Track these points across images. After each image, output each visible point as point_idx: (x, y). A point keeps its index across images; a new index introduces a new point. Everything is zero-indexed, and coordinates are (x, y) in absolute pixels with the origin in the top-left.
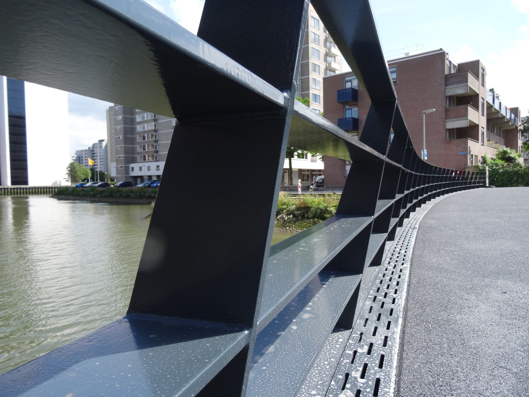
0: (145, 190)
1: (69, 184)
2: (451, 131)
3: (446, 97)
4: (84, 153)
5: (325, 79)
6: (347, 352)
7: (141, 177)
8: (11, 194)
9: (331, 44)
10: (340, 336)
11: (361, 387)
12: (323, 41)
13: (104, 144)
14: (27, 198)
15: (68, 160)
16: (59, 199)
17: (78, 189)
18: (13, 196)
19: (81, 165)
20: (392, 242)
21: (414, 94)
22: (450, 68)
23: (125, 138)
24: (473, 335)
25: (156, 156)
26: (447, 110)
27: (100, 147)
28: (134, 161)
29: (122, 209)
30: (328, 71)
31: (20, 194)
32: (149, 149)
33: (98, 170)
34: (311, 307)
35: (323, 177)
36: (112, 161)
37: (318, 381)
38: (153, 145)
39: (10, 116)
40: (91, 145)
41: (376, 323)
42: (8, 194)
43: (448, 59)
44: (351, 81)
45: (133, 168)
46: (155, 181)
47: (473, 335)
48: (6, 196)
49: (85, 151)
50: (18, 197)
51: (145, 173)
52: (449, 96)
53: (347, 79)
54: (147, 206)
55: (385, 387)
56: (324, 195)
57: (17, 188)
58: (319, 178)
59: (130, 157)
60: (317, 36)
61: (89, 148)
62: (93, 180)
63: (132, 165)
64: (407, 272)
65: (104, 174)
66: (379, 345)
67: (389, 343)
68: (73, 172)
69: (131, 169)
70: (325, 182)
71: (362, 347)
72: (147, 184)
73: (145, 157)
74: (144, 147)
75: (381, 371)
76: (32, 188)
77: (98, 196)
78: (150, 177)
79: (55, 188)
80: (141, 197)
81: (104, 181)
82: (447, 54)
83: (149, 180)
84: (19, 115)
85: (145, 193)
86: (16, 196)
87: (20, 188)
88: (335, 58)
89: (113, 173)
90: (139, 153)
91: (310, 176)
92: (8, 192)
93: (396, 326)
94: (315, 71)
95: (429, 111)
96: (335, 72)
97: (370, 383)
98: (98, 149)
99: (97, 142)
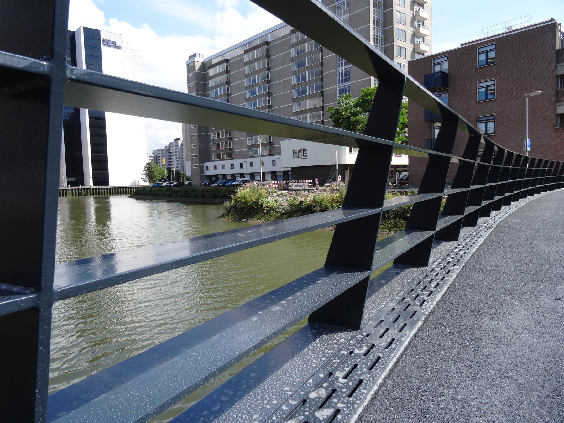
0: (220, 189)
1: (146, 184)
3: (558, 76)
4: (160, 152)
5: (409, 63)
6: (342, 352)
7: (216, 176)
8: (93, 195)
9: (419, 23)
10: (344, 336)
11: (338, 387)
12: (410, 20)
13: (180, 143)
14: (108, 198)
15: (146, 160)
16: (137, 199)
17: (155, 189)
18: (95, 196)
19: (159, 164)
20: (455, 242)
21: (516, 75)
23: (200, 136)
24: (493, 342)
25: (230, 154)
26: (558, 92)
27: (176, 146)
28: (208, 159)
29: (198, 208)
30: (416, 54)
31: (102, 194)
32: (224, 146)
33: (175, 169)
34: (289, 301)
35: (407, 173)
36: (187, 160)
37: (297, 378)
38: (227, 143)
39: (90, 117)
40: (167, 145)
41: (389, 325)
42: (90, 195)
43: (560, 31)
44: (440, 64)
45: (207, 167)
46: (229, 180)
47: (493, 342)
48: (89, 197)
49: (162, 150)
50: (99, 198)
51: (219, 171)
52: (562, 75)
54: (221, 206)
55: (365, 388)
56: (406, 193)
57: (99, 189)
58: (403, 174)
59: (205, 155)
60: (403, 15)
61: (166, 147)
62: (170, 180)
63: (207, 164)
64: (454, 275)
65: (180, 173)
66: (381, 347)
67: (393, 345)
68: (150, 171)
69: (205, 168)
70: (409, 178)
71: (360, 348)
72: (221, 183)
73: (219, 155)
75: (369, 373)
76: (112, 188)
77: (174, 195)
78: (224, 176)
79: (133, 188)
80: (216, 197)
81: (180, 180)
82: (560, 24)
83: (223, 180)
84: (99, 116)
85: (219, 192)
86: (98, 196)
87: (102, 189)
88: (424, 38)
89: (189, 173)
92: (90, 192)
93: (411, 329)
94: (400, 55)
96: (423, 54)
97: (351, 383)
98: (174, 148)
99: (173, 141)
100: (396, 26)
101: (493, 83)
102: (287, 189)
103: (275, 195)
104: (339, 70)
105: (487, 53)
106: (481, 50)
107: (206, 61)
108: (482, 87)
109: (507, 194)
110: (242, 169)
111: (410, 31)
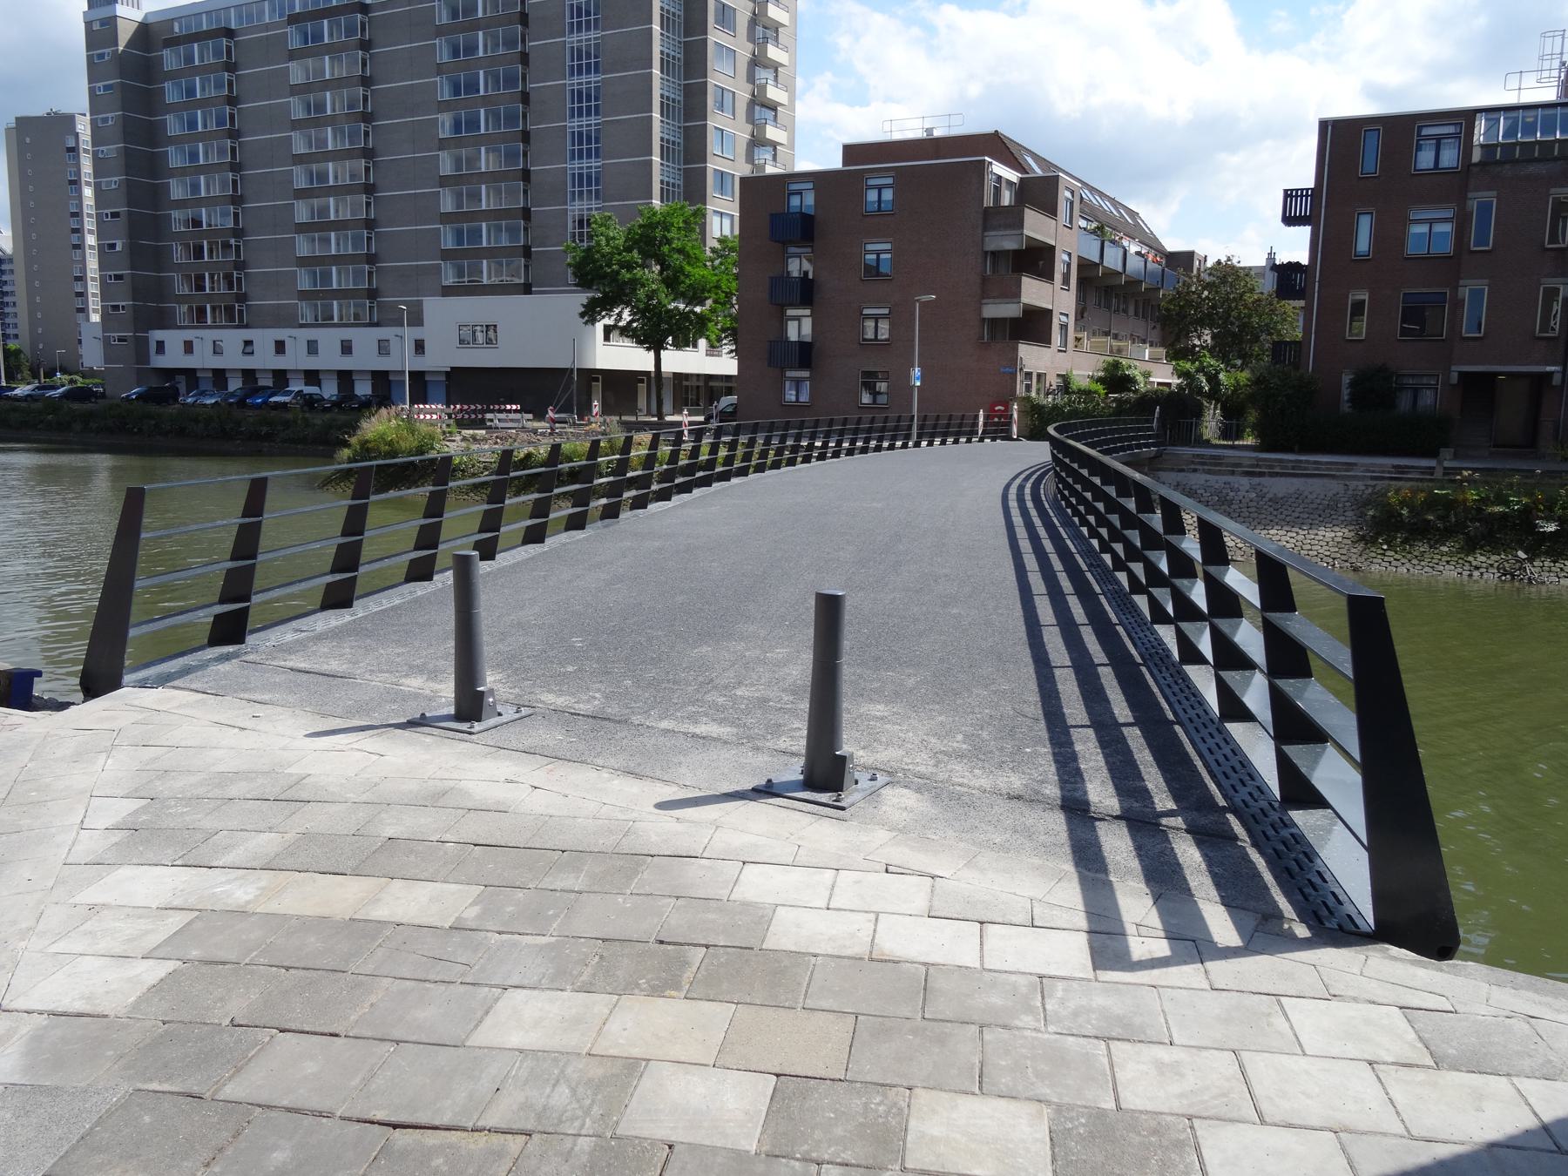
2: (994, 323)
7: (190, 373)
22: (997, 191)
23: (134, 250)
26: (984, 280)
28: (165, 321)
35: (733, 399)
51: (203, 359)
53: (794, 187)
58: (727, 401)
63: (157, 335)
69: (153, 347)
73: (201, 312)
74: (200, 278)
78: (249, 375)
90: (182, 299)
91: (702, 391)
95: (925, 298)
100: (716, 36)
101: (888, 246)
102: (481, 424)
103: (458, 438)
104: (574, 124)
105: (880, 189)
106: (871, 182)
107: (151, 20)
108: (871, 252)
109: (1075, 466)
110: (280, 358)
111: (744, 51)
